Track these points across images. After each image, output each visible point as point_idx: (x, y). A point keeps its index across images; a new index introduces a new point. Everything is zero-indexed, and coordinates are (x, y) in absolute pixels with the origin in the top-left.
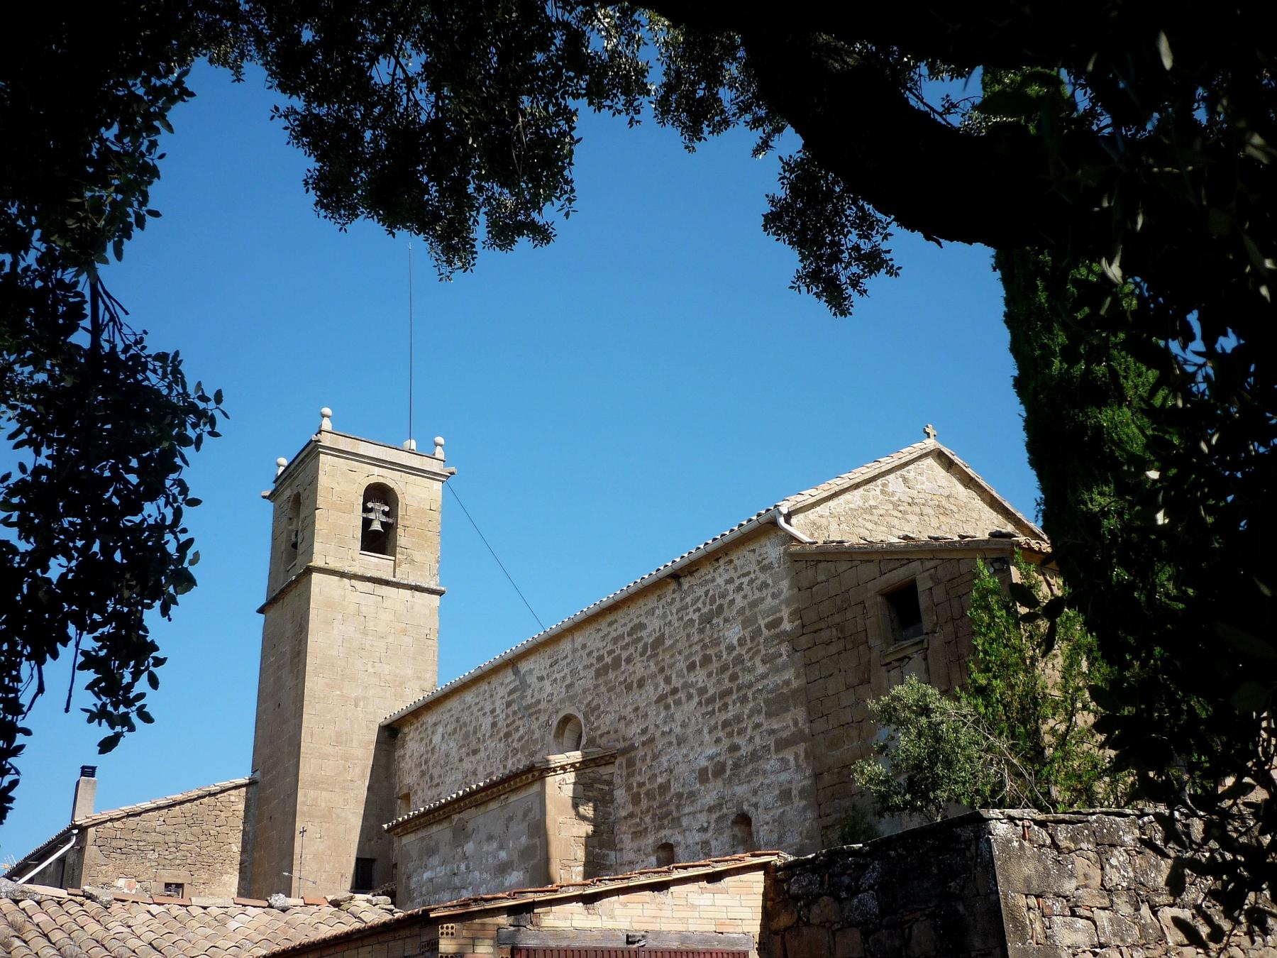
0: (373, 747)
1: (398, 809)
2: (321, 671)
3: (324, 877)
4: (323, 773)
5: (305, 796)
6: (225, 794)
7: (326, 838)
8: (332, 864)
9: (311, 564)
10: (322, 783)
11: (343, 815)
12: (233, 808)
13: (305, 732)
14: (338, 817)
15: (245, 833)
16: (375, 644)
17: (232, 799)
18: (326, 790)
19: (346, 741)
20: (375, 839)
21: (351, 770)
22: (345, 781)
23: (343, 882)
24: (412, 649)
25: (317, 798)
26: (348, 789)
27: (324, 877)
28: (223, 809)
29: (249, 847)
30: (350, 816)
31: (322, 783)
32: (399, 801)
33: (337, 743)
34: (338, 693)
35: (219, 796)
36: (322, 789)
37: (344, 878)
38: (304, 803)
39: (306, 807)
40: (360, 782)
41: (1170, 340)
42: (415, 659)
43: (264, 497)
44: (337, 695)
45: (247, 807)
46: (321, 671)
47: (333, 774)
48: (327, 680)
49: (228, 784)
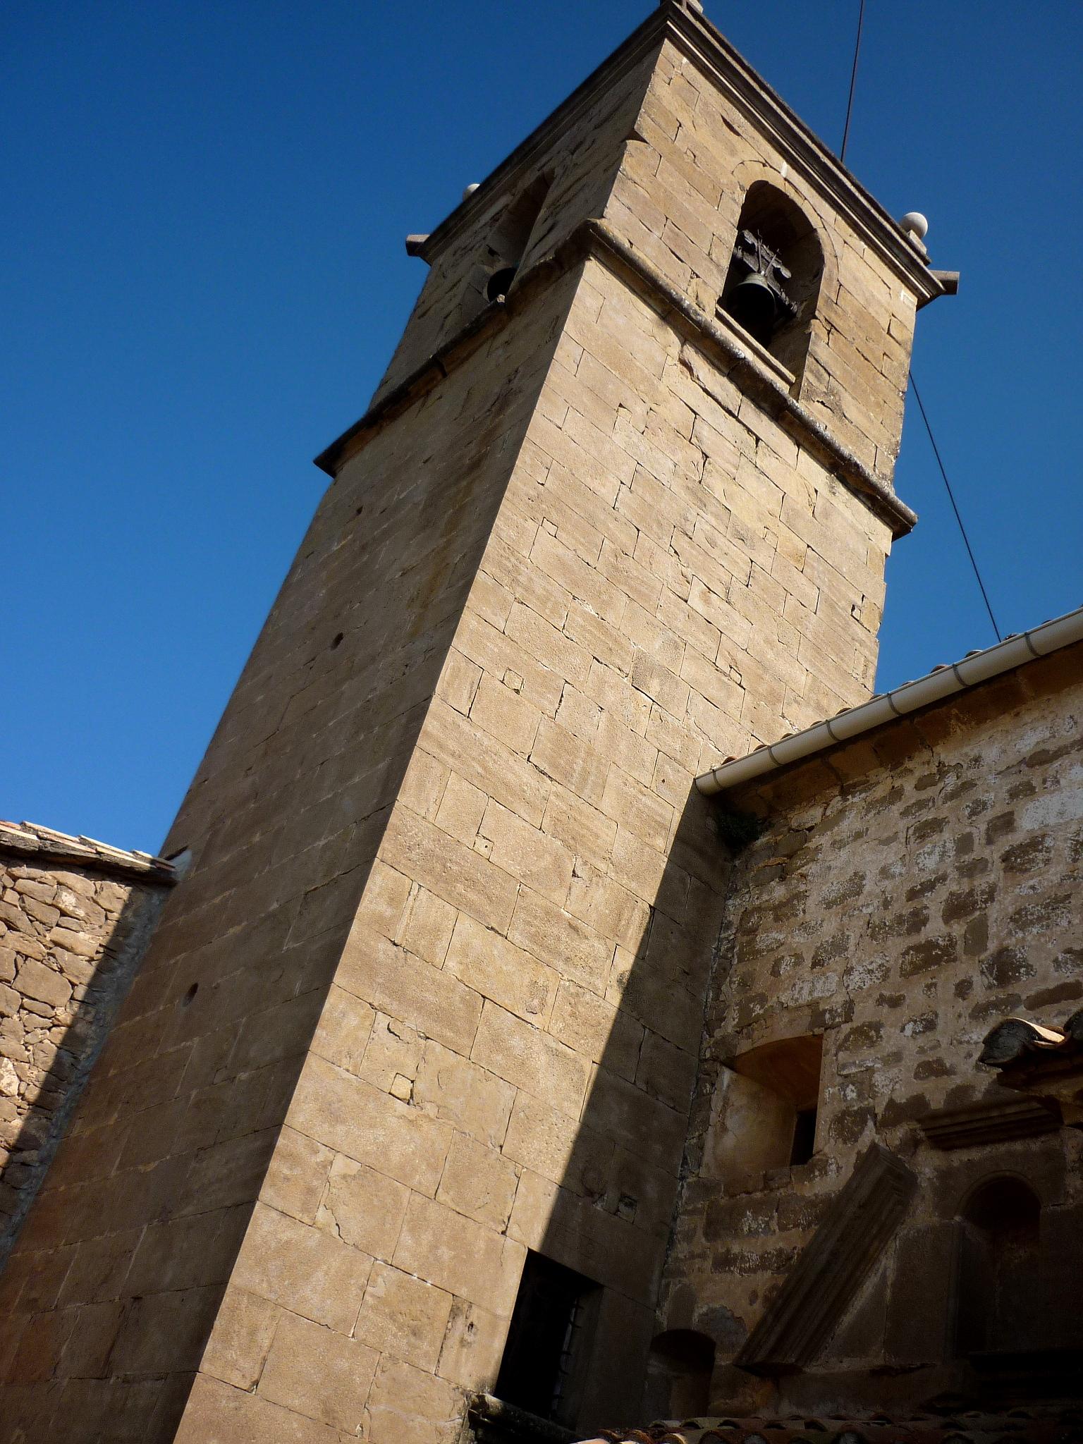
0: (663, 843)
1: (717, 1103)
2: (555, 517)
3: (380, 1289)
4: (481, 845)
5: (394, 900)
6: (48, 875)
7: (431, 1110)
8: (427, 1237)
9: (598, 221)
10: (471, 882)
11: (516, 1042)
12: (57, 934)
13: (456, 673)
14: (497, 1042)
15: (71, 1041)
16: (721, 541)
17: (67, 900)
18: (478, 915)
19: (584, 780)
20: (611, 1195)
21: (578, 885)
22: (551, 915)
23: (453, 1341)
24: (814, 618)
25: (436, 931)
26: (556, 953)
27: (380, 1289)
28: (22, 922)
29: (62, 1097)
30: (541, 1060)
31: (471, 882)
32: (727, 1076)
33: (555, 766)
34: (590, 610)
35: (23, 870)
36: (461, 905)
37: (461, 1323)
38: (383, 926)
39: (384, 946)
40: (600, 948)
41: (1000, 1070)
42: (817, 649)
43: (413, 249)
44: (584, 614)
45: (110, 952)
46: (555, 517)
47: (515, 870)
48: (561, 550)
49: (72, 843)
